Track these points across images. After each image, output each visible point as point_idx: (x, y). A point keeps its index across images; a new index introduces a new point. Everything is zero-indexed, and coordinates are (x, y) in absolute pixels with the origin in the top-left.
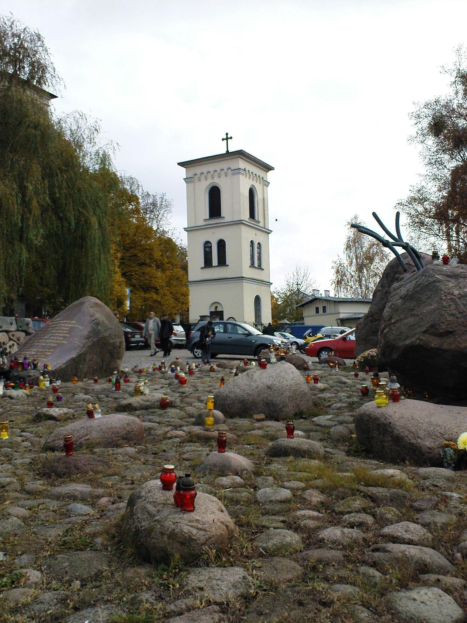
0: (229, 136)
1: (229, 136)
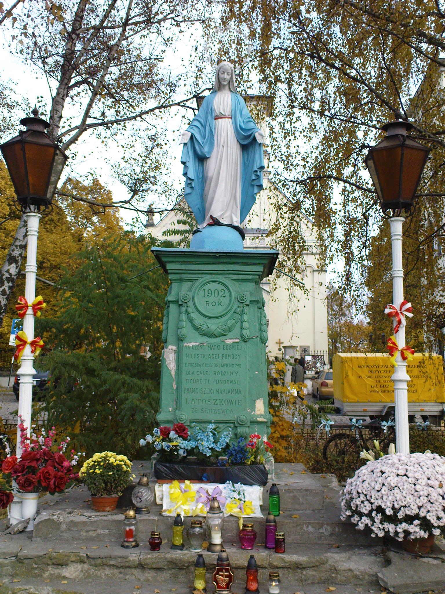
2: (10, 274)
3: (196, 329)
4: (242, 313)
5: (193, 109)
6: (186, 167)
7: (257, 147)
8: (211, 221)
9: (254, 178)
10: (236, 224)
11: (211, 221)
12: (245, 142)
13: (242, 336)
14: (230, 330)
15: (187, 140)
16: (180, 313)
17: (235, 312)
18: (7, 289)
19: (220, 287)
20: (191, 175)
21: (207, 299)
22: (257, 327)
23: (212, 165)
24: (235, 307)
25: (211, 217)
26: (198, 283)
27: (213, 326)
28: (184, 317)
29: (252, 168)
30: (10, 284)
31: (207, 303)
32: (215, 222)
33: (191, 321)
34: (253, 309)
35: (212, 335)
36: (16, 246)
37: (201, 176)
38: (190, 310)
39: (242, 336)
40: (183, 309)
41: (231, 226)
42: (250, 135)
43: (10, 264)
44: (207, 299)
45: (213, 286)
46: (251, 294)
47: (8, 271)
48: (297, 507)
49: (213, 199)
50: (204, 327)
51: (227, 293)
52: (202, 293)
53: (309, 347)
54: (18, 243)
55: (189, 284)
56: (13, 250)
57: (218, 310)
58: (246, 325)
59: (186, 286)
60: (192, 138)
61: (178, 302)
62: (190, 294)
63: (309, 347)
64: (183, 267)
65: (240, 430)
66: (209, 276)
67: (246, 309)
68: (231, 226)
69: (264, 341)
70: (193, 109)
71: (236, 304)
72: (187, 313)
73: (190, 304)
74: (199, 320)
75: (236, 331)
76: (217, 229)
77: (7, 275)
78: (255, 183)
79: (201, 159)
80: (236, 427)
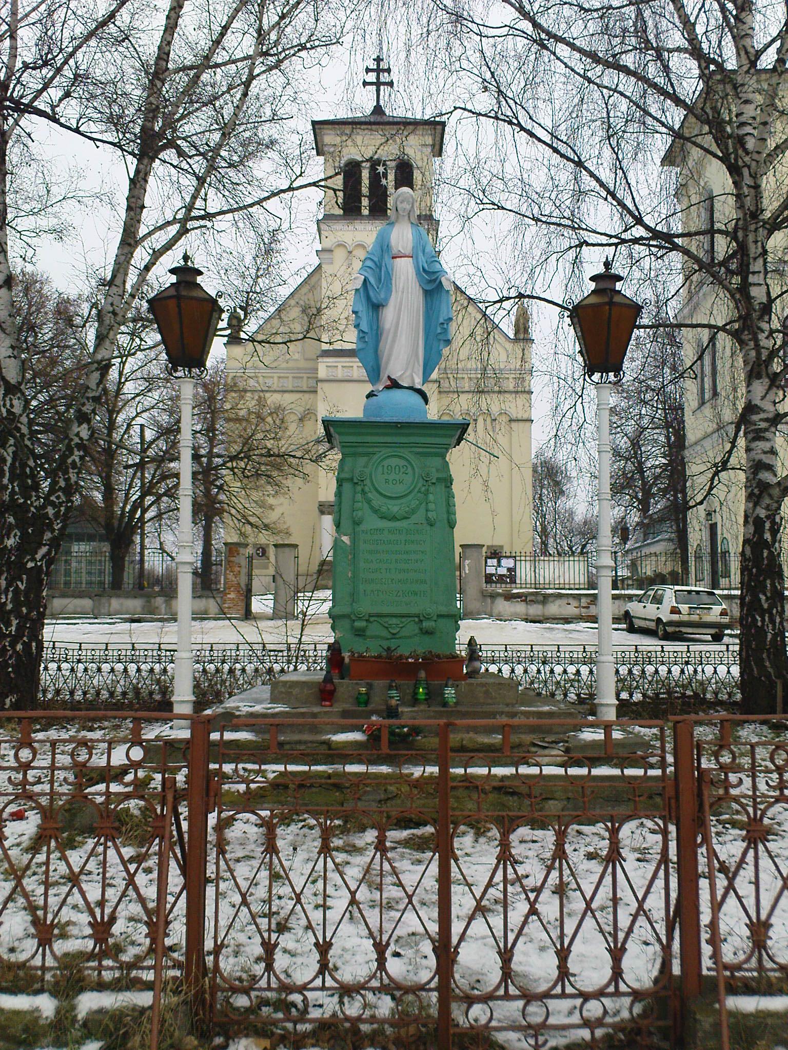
0: (373, 66)
1: (373, 66)
2: (81, 439)
3: (375, 511)
4: (427, 493)
5: (335, 190)
6: (357, 317)
7: (444, 294)
8: (389, 383)
9: (439, 331)
10: (418, 386)
11: (389, 383)
12: (428, 287)
13: (427, 519)
14: (414, 511)
15: (359, 284)
16: (355, 493)
17: (419, 492)
18: (77, 459)
19: (402, 462)
20: (364, 326)
21: (386, 476)
22: (445, 509)
23: (389, 315)
24: (420, 485)
25: (389, 377)
26: (376, 457)
27: (394, 508)
28: (359, 497)
29: (438, 318)
30: (82, 453)
31: (387, 481)
32: (394, 385)
33: (369, 502)
34: (440, 488)
35: (394, 518)
36: (88, 398)
37: (375, 327)
38: (367, 489)
39: (427, 519)
40: (359, 488)
41: (411, 388)
42: (435, 280)
43: (80, 425)
44: (386, 476)
45: (394, 462)
46: (437, 471)
47: (78, 435)
48: (490, 701)
49: (390, 356)
50: (384, 509)
51: (410, 470)
52: (380, 468)
53: (502, 547)
54: (91, 394)
55: (365, 459)
56: (84, 404)
57: (400, 489)
58: (431, 506)
59: (362, 461)
60: (365, 281)
61: (352, 479)
62: (367, 470)
63: (502, 547)
64: (359, 439)
65: (425, 624)
66: (389, 450)
67: (432, 489)
68: (411, 388)
69: (452, 525)
70: (335, 190)
71: (421, 482)
72: (363, 492)
73: (368, 482)
74: (377, 501)
75: (422, 511)
76: (396, 394)
77: (77, 440)
78: (441, 337)
79: (376, 307)
80: (421, 621)
